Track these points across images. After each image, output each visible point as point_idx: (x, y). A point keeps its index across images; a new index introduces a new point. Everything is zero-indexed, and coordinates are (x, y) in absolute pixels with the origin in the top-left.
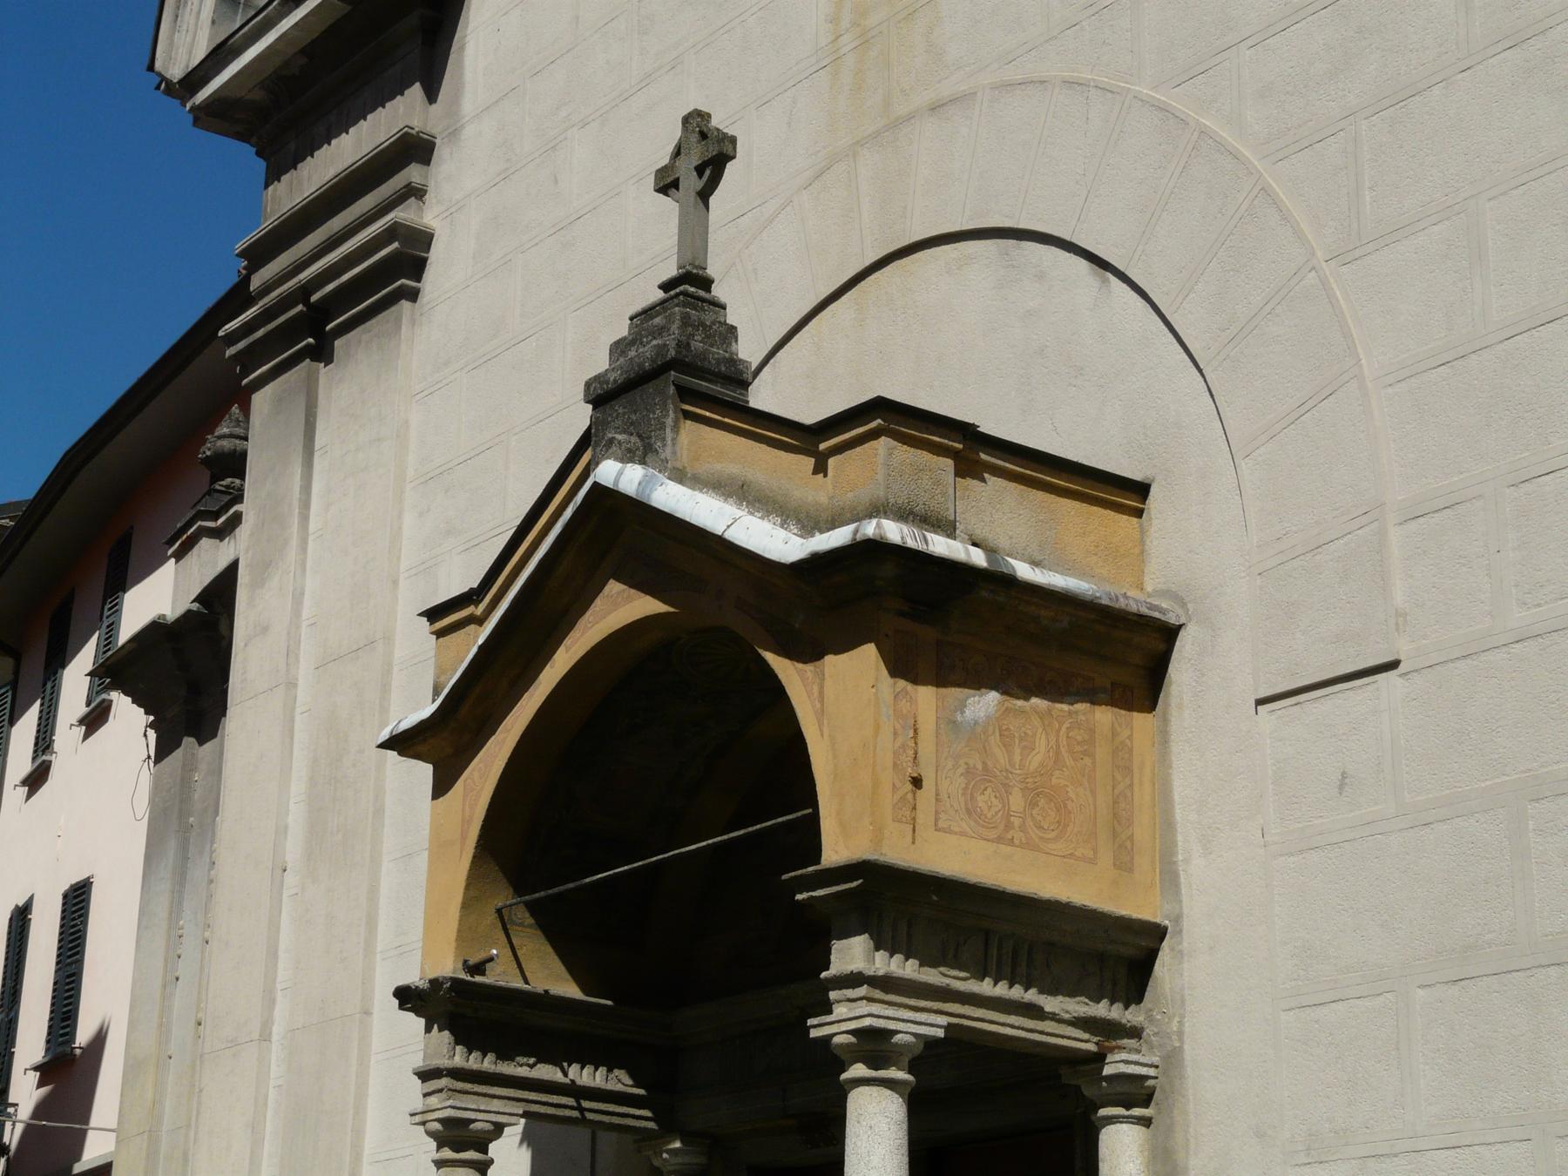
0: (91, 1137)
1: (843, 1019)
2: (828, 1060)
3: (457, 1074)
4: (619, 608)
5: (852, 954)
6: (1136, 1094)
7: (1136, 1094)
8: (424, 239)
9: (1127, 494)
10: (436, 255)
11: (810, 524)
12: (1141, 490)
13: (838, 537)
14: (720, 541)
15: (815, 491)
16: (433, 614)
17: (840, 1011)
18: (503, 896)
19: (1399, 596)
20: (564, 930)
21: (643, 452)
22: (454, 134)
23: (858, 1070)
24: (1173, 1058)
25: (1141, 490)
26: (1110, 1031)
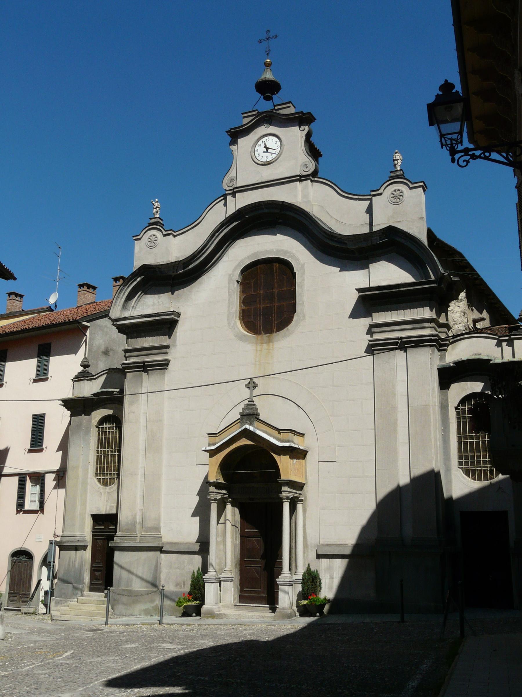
0: (5, 468)
1: (284, 495)
2: (282, 499)
3: (216, 492)
4: (244, 442)
5: (285, 488)
6: (301, 501)
7: (301, 501)
8: (169, 361)
9: (302, 435)
10: (170, 363)
11: (281, 441)
12: (304, 435)
13: (287, 444)
14: (268, 441)
15: (279, 436)
16: (208, 434)
17: (283, 494)
18: (219, 471)
19: (337, 454)
20: (224, 476)
21: (251, 424)
22: (175, 346)
23: (286, 500)
24: (306, 497)
25: (304, 435)
26: (300, 494)
